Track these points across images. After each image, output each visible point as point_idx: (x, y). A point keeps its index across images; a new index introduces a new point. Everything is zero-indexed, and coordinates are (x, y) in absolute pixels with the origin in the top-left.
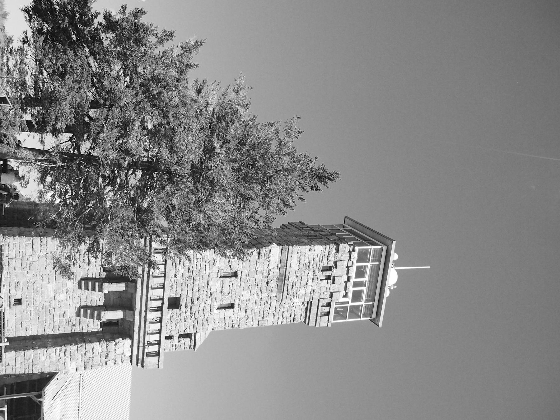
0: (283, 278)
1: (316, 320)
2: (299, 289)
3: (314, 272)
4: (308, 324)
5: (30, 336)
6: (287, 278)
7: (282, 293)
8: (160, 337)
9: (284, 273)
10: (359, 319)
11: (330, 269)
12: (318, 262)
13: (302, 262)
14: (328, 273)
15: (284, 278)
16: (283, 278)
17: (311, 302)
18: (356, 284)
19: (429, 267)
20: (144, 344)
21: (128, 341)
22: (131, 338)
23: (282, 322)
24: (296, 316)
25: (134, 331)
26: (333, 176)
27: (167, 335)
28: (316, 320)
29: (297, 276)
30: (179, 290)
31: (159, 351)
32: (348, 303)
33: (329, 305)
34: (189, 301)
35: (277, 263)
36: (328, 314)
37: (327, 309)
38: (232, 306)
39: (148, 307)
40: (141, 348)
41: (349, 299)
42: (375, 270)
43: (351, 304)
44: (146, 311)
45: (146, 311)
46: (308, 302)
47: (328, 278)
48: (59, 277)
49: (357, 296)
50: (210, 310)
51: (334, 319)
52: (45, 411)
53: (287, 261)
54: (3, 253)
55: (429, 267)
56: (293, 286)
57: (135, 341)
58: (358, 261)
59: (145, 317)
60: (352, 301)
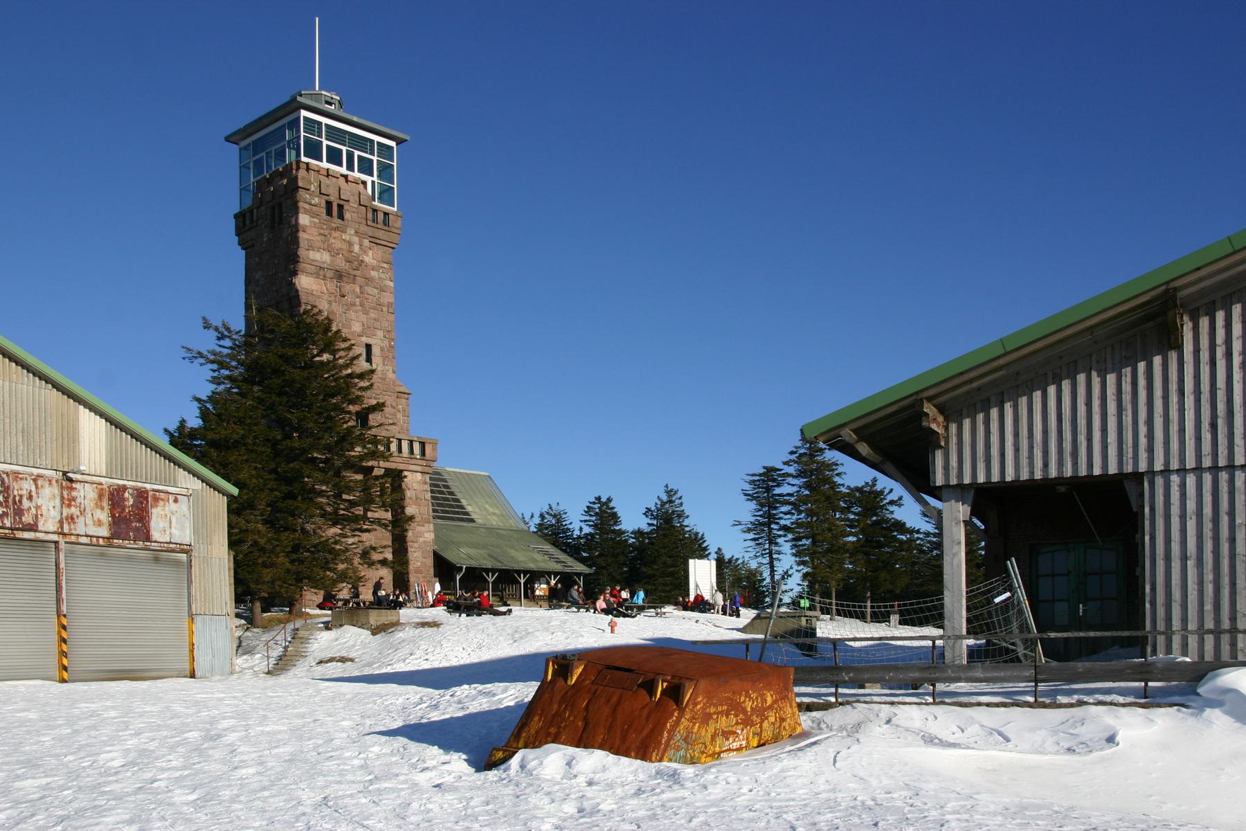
36: (386, 214)
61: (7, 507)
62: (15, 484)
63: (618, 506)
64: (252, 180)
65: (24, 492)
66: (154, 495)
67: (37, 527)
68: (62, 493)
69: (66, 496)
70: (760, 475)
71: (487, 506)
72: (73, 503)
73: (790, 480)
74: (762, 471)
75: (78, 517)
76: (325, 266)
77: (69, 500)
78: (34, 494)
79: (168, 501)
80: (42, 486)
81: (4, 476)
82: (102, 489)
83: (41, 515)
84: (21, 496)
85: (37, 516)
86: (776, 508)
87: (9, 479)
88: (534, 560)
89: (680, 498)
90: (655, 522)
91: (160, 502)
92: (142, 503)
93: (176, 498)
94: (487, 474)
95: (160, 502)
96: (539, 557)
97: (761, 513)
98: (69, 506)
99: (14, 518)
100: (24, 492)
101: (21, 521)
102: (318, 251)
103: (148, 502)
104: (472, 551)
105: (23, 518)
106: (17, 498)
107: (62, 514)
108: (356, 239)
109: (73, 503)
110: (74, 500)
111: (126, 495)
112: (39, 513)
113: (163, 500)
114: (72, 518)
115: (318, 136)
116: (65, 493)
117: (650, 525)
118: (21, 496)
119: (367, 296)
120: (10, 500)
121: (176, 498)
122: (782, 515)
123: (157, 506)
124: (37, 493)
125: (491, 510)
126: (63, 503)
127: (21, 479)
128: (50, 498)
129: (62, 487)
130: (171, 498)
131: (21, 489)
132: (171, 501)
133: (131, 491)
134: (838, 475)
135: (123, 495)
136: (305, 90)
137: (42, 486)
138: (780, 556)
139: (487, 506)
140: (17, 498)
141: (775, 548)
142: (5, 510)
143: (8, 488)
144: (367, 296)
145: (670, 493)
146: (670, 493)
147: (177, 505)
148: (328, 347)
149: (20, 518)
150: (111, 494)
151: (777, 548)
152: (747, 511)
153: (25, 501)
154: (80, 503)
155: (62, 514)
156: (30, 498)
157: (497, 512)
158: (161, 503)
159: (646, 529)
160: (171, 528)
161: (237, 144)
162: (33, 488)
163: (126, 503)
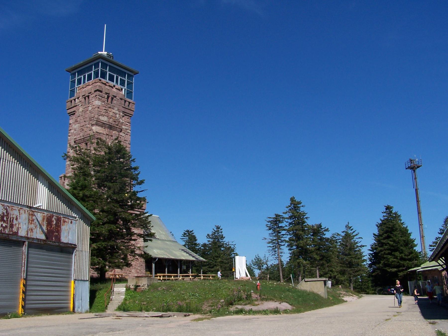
0: (111, 127)
2: (116, 118)
3: (110, 108)
4: (132, 115)
5: (158, 249)
6: (110, 124)
11: (108, 97)
13: (104, 114)
14: (110, 98)
17: (123, 111)
19: (105, 25)
23: (130, 130)
26: (292, 200)
29: (111, 118)
32: (125, 89)
35: (103, 129)
36: (129, 103)
37: (127, 103)
43: (126, 88)
46: (123, 114)
47: (112, 99)
52: (163, 257)
54: (290, 202)
55: (105, 25)
56: (115, 122)
61: (7, 223)
62: (11, 212)
63: (196, 234)
64: (76, 86)
65: (15, 216)
66: (64, 219)
67: (18, 234)
68: (29, 217)
69: (30, 219)
70: (273, 218)
71: (160, 231)
72: (33, 222)
73: (286, 220)
74: (275, 216)
75: (34, 229)
76: (106, 123)
77: (31, 221)
78: (18, 217)
79: (69, 223)
80: (22, 213)
81: (8, 208)
82: (44, 216)
83: (20, 228)
84: (13, 218)
85: (18, 228)
86: (280, 233)
87: (9, 209)
88: (183, 256)
89: (222, 229)
90: (211, 240)
91: (66, 222)
92: (59, 223)
93: (71, 221)
94: (158, 216)
95: (66, 222)
96: (185, 254)
97: (274, 235)
98: (31, 223)
99: (10, 229)
100: (15, 216)
101: (12, 231)
102: (104, 117)
103: (61, 223)
104: (159, 251)
105: (13, 229)
106: (12, 219)
107: (28, 228)
108: (117, 112)
109: (33, 222)
110: (33, 221)
111: (53, 219)
112: (19, 227)
113: (66, 222)
114: (32, 230)
115: (106, 70)
116: (30, 217)
117: (209, 241)
118: (13, 218)
119: (121, 136)
120: (9, 220)
121: (71, 221)
122: (282, 236)
123: (64, 225)
124: (20, 217)
125: (161, 232)
126: (29, 222)
127: (14, 209)
128: (24, 220)
129: (29, 215)
130: (70, 221)
131: (14, 215)
132: (70, 222)
133: (55, 217)
134: (306, 218)
135: (52, 219)
136: (100, 52)
137: (22, 213)
138: (282, 254)
139: (160, 231)
140: (12, 219)
141: (280, 251)
142: (6, 225)
143: (9, 214)
144: (121, 136)
145: (218, 228)
146: (218, 228)
147: (72, 225)
148: (123, 157)
149: (12, 229)
150: (48, 218)
151: (281, 251)
152: (267, 234)
153: (14, 220)
154: (36, 223)
155: (28, 228)
156: (17, 219)
157: (164, 233)
158: (66, 223)
159: (207, 243)
160: (69, 235)
161: (70, 72)
162: (18, 215)
163: (53, 223)
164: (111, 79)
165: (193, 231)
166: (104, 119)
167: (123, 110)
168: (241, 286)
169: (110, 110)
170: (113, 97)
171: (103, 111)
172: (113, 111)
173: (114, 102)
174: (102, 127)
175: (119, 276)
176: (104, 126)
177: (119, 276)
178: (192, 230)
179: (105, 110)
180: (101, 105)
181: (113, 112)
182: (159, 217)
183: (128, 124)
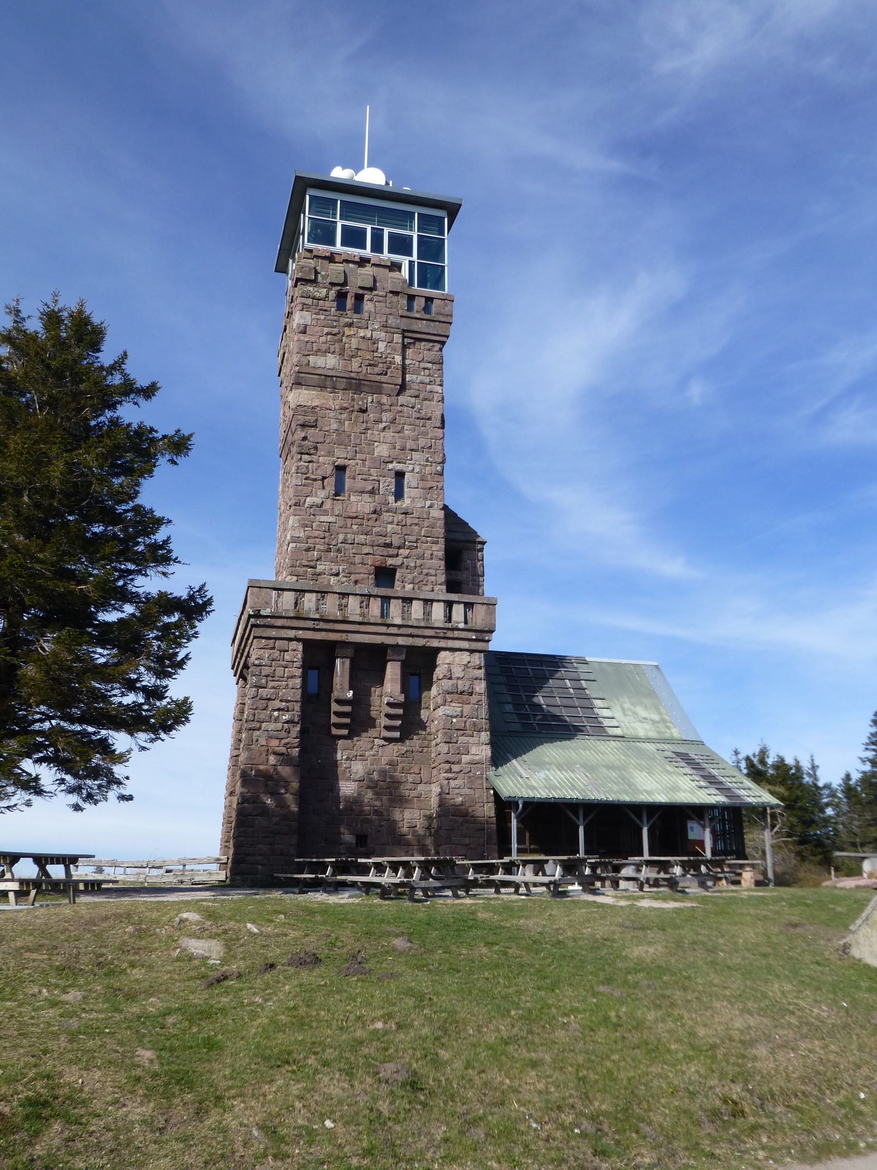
0: (355, 384)
1: (439, 322)
6: (353, 375)
7: (384, 385)
8: (458, 602)
9: (345, 380)
10: (446, 241)
12: (329, 318)
15: (354, 381)
16: (355, 384)
17: (404, 330)
18: (377, 247)
20: (448, 629)
21: (443, 658)
22: (438, 650)
24: (430, 359)
25: (424, 647)
27: (444, 591)
28: (439, 322)
30: (364, 569)
31: (444, 601)
32: (411, 263)
33: (411, 298)
34: (385, 551)
36: (429, 300)
37: (419, 303)
38: (400, 475)
39: (380, 621)
40: (456, 634)
41: (405, 261)
42: (349, 211)
43: (415, 257)
44: (389, 626)
45: (389, 626)
47: (359, 298)
48: (806, 765)
49: (400, 245)
50: (404, 513)
51: (364, 248)
53: (321, 375)
57: (442, 644)
58: (332, 243)
59: (399, 626)
60: (411, 255)
164: (354, 238)
165: (149, 392)
166: (329, 362)
167: (404, 324)
168: (523, 1133)
169: (348, 332)
170: (361, 292)
171: (323, 339)
172: (362, 335)
173: (368, 306)
174: (323, 387)
175: (50, 868)
176: (328, 383)
177: (50, 868)
178: (142, 382)
179: (329, 337)
180: (314, 322)
181: (363, 338)
182: (657, 667)
183: (430, 366)
